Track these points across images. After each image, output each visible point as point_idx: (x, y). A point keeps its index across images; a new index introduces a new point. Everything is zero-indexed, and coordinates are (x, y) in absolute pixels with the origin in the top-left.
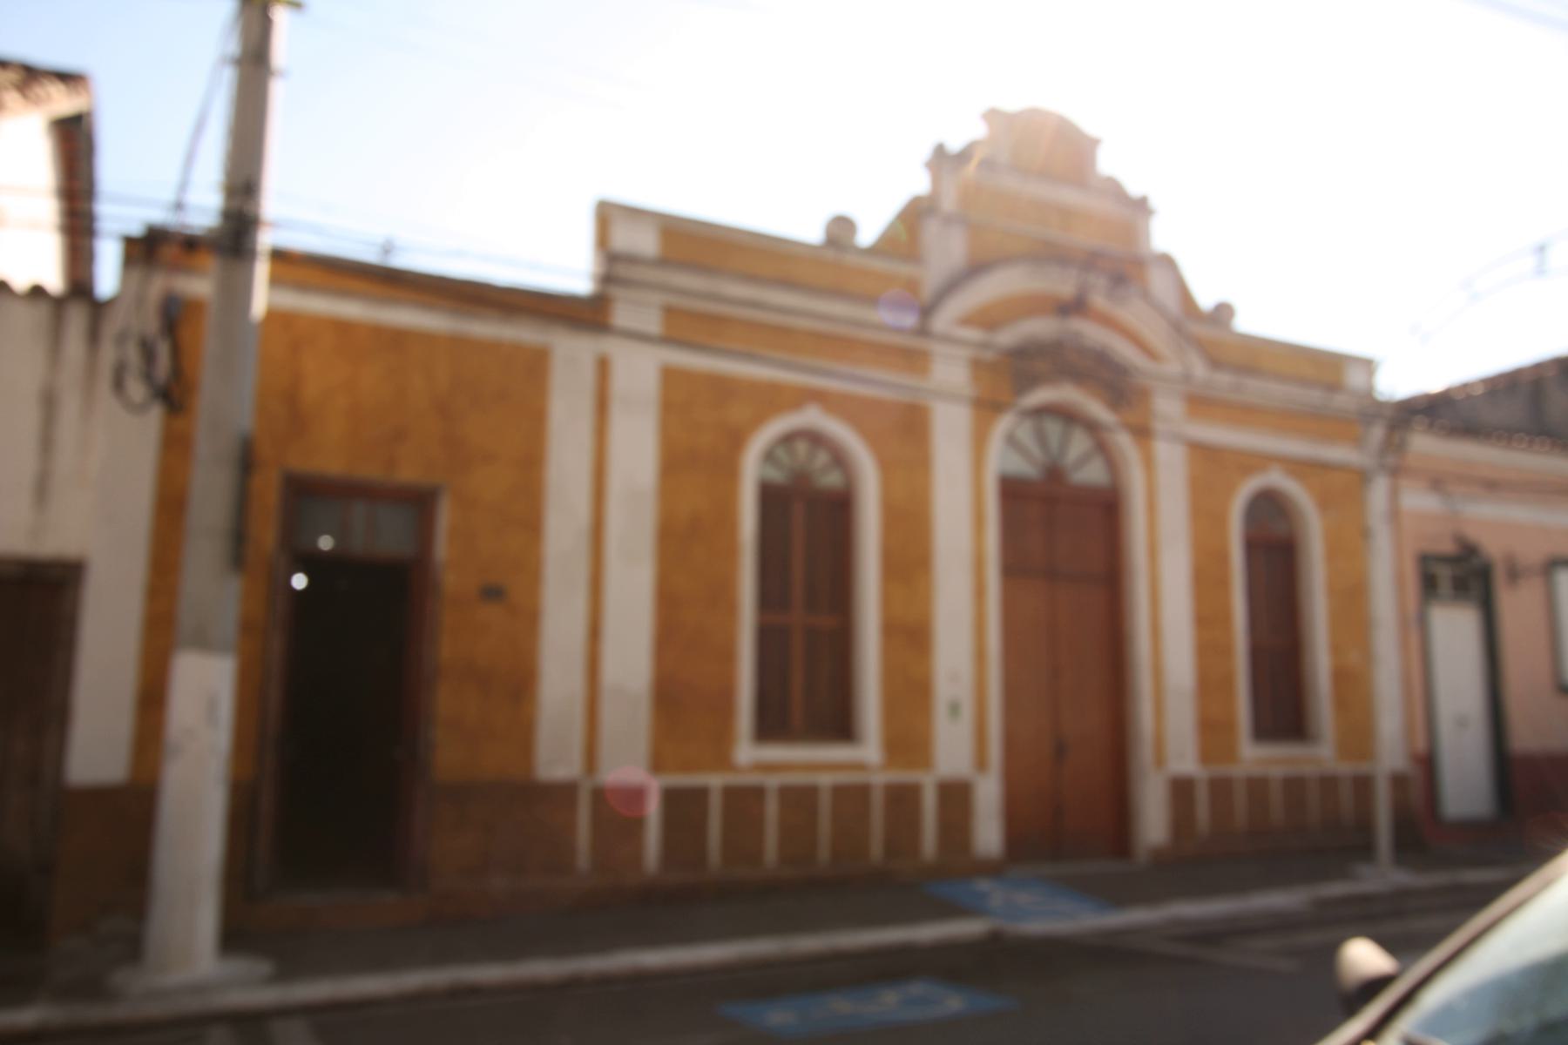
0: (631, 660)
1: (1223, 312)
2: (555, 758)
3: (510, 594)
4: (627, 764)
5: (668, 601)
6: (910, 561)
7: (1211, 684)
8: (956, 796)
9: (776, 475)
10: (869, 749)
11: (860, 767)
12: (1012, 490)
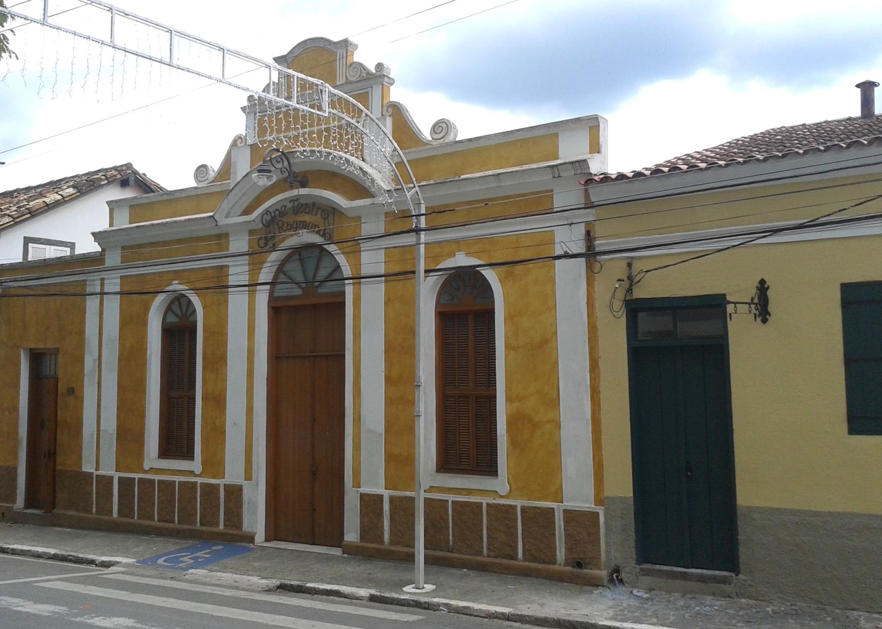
0: (110, 423)
1: (442, 127)
2: (88, 467)
3: (75, 392)
4: (109, 470)
5: (122, 388)
6: (217, 362)
7: (399, 426)
8: (234, 493)
9: (172, 319)
10: (196, 465)
11: (192, 473)
12: (276, 310)
